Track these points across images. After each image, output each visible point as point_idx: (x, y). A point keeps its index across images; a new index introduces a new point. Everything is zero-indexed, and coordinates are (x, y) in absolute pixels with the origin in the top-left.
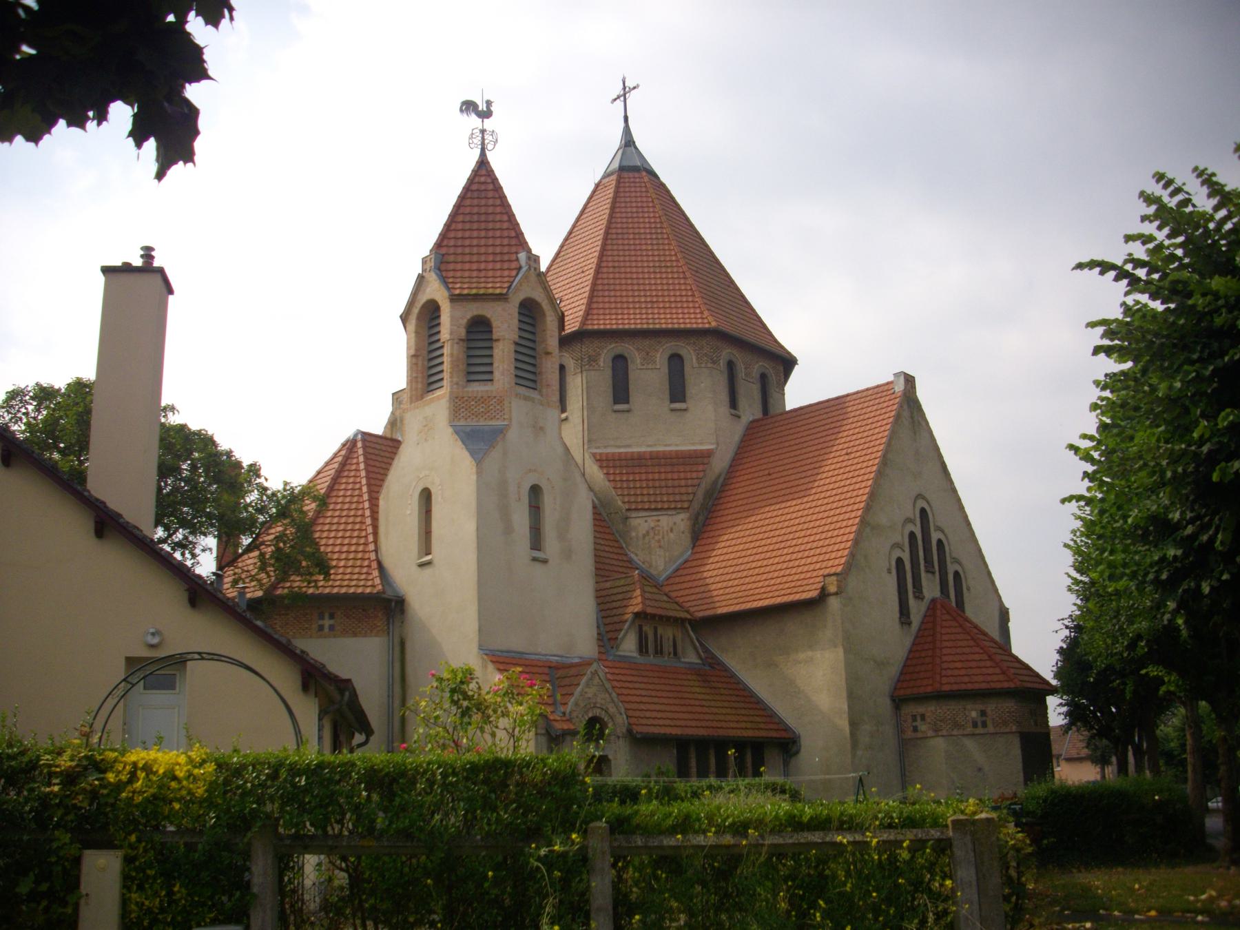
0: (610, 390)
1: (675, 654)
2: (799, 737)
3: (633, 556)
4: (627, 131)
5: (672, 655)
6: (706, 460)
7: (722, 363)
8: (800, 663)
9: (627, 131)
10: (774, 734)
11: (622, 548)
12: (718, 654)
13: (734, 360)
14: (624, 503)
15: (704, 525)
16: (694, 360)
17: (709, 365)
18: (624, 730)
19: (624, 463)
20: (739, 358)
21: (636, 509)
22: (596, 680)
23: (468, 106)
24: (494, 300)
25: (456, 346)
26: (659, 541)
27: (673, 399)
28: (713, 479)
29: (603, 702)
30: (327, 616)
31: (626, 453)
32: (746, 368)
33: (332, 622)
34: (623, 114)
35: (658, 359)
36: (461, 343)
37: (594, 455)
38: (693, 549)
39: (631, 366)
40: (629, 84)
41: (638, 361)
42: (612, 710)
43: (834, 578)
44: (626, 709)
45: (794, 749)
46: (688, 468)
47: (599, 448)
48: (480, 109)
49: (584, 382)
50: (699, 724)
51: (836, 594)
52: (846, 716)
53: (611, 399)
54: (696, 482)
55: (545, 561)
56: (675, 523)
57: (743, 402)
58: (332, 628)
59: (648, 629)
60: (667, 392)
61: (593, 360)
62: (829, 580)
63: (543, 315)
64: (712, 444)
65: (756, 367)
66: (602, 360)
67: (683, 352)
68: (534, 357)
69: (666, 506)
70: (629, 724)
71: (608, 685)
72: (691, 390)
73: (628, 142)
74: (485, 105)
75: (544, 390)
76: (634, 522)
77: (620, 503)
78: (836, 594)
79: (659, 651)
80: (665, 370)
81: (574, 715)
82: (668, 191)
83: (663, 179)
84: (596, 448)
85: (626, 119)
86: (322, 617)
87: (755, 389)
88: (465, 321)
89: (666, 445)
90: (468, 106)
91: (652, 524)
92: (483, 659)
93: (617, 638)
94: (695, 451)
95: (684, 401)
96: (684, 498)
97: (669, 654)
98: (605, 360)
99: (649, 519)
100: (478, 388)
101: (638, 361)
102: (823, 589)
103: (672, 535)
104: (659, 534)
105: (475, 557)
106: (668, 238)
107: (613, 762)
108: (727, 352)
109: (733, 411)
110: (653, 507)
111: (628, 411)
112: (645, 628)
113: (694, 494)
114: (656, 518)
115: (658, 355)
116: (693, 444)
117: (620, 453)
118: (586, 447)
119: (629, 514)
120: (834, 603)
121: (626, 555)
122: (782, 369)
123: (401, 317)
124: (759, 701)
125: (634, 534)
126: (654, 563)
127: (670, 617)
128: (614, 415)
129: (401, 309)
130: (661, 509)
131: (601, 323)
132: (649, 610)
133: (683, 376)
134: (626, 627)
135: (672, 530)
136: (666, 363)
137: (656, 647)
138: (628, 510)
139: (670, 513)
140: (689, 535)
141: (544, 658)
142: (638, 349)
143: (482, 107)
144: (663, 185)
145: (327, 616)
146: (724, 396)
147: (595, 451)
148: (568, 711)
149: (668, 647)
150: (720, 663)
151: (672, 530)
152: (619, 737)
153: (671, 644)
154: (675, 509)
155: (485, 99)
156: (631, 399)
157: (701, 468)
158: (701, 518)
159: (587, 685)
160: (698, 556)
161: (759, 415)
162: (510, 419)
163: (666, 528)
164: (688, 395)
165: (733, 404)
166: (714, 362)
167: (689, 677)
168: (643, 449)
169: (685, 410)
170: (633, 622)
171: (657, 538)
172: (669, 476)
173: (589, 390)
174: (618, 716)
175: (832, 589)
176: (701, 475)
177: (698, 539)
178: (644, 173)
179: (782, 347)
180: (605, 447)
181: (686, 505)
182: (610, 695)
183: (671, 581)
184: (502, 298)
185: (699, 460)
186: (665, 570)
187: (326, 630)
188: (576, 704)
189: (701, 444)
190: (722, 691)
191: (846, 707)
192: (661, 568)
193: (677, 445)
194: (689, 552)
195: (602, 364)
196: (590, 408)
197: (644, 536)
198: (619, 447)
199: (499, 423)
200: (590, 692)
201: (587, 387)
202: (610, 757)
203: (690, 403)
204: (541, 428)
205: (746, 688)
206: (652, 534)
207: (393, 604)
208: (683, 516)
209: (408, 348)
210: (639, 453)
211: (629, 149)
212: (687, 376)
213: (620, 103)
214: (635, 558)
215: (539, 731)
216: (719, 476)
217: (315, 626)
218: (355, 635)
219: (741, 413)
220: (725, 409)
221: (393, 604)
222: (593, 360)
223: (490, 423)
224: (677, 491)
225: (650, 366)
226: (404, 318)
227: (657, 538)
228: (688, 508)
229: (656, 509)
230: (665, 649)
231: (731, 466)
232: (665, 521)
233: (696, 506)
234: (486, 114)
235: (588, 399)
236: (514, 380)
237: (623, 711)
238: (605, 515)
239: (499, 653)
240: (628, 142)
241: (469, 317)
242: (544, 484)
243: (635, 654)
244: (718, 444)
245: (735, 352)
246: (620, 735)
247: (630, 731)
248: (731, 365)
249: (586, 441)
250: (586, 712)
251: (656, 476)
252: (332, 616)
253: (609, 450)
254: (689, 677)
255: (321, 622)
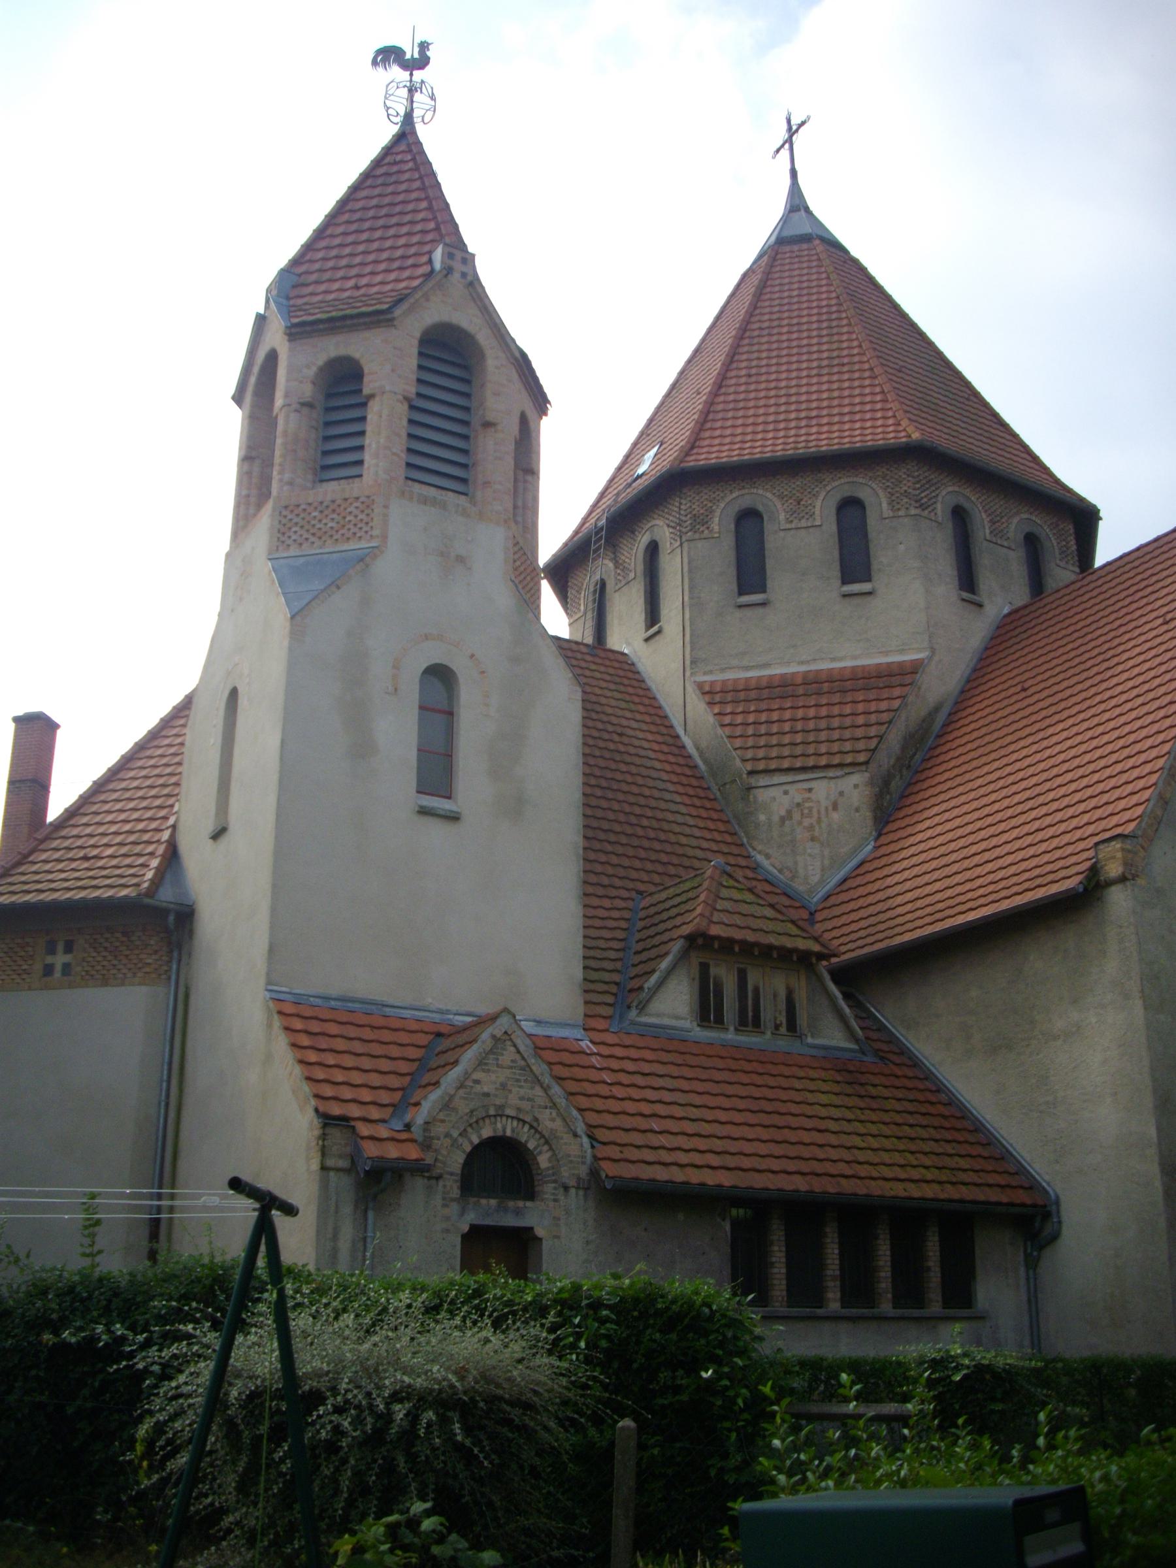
0: (732, 572)
1: (792, 1026)
2: (1057, 1202)
3: (760, 858)
4: (795, 191)
5: (783, 1030)
6: (908, 679)
7: (941, 510)
8: (1056, 1038)
9: (795, 191)
10: (994, 1196)
11: (742, 845)
12: (899, 1032)
13: (967, 505)
14: (744, 761)
15: (903, 797)
16: (885, 505)
17: (913, 511)
18: (583, 1171)
19: (753, 695)
20: (980, 507)
21: (766, 771)
22: (508, 1055)
23: (388, 55)
24: (368, 326)
25: (293, 416)
26: (811, 828)
27: (847, 577)
28: (923, 713)
29: (525, 1105)
30: (60, 947)
31: (759, 678)
32: (992, 522)
33: (67, 958)
34: (789, 167)
35: (817, 511)
36: (305, 410)
37: (700, 686)
38: (876, 839)
39: (768, 527)
40: (795, 121)
41: (782, 516)
42: (549, 1122)
43: (1117, 845)
44: (589, 1126)
45: (1048, 1230)
46: (872, 695)
47: (711, 672)
48: (408, 56)
49: (686, 560)
50: (791, 1166)
51: (1123, 879)
52: (1152, 1152)
53: (735, 587)
54: (885, 717)
55: (453, 818)
56: (841, 794)
57: (987, 581)
58: (67, 968)
59: (725, 974)
60: (836, 566)
61: (700, 522)
62: (1106, 851)
63: (481, 355)
64: (920, 650)
65: (1015, 520)
66: (716, 520)
67: (864, 494)
68: (466, 437)
69: (823, 761)
70: (596, 1158)
71: (539, 1068)
72: (881, 557)
73: (797, 204)
74: (416, 50)
75: (479, 494)
76: (762, 795)
77: (738, 762)
78: (1123, 879)
79: (750, 1020)
80: (832, 527)
81: (439, 1129)
82: (862, 270)
83: (854, 252)
84: (705, 674)
85: (794, 173)
86: (52, 951)
87: (1016, 562)
88: (314, 369)
89: (833, 660)
90: (388, 55)
91: (798, 799)
92: (268, 1007)
93: (641, 988)
94: (889, 664)
95: (869, 580)
96: (861, 745)
97: (777, 1027)
98: (721, 519)
99: (791, 789)
100: (332, 491)
101: (782, 516)
102: (1094, 871)
103: (835, 816)
104: (810, 816)
105: (272, 799)
106: (849, 325)
107: (546, 1245)
108: (949, 493)
109: (965, 595)
110: (798, 765)
111: (763, 604)
112: (713, 971)
113: (881, 737)
114: (806, 785)
115: (818, 504)
116: (886, 653)
117: (747, 679)
118: (688, 674)
119: (753, 781)
120: (1119, 900)
121: (749, 857)
122: (1070, 528)
123: (233, 398)
124: (978, 1127)
125: (762, 818)
126: (801, 872)
127: (771, 947)
128: (739, 614)
129: (232, 387)
130: (815, 768)
131: (709, 456)
132: (715, 930)
133: (866, 535)
134: (664, 964)
135: (835, 807)
136: (833, 519)
137: (743, 1011)
138: (751, 773)
139: (831, 773)
140: (869, 814)
141: (437, 1017)
142: (781, 497)
143: (411, 52)
144: (856, 263)
145: (60, 947)
146: (946, 565)
147: (701, 678)
148: (420, 1121)
149: (774, 1011)
150: (903, 1051)
151: (835, 807)
152: (566, 1188)
153: (782, 1006)
154: (840, 765)
155: (417, 41)
156: (769, 584)
157: (897, 692)
158: (896, 784)
159: (481, 1064)
160: (883, 851)
161: (1019, 595)
162: (384, 537)
163: (824, 803)
164: (875, 566)
165: (968, 580)
166: (923, 507)
167: (812, 1074)
168: (793, 669)
169: (870, 593)
170: (684, 955)
171: (806, 822)
172: (836, 710)
173: (692, 571)
174: (567, 1138)
175: (1113, 870)
176: (896, 703)
177: (887, 823)
178: (817, 242)
179: (1057, 481)
180: (723, 670)
181: (862, 758)
182: (546, 1090)
183: (832, 901)
184: (379, 319)
185: (896, 680)
186: (822, 882)
187: (58, 974)
188: (447, 1105)
189: (902, 651)
190: (890, 1104)
191: (1153, 1132)
192: (815, 879)
193: (854, 658)
194: (870, 847)
195: (716, 528)
196: (695, 604)
197: (783, 820)
198: (747, 668)
199: (363, 544)
200: (489, 1082)
201: (690, 571)
202: (540, 1232)
203: (879, 582)
204: (460, 559)
205: (952, 1102)
206: (796, 816)
207: (171, 918)
208: (858, 778)
209: (240, 449)
210: (782, 675)
211: (795, 216)
212: (872, 534)
213: (785, 153)
214: (766, 863)
215: (330, 1163)
216: (937, 709)
217: (38, 967)
218: (105, 982)
219: (984, 598)
220: (947, 590)
221: (171, 918)
222: (700, 522)
223: (346, 547)
224: (847, 734)
225: (803, 523)
226: (238, 398)
227: (806, 822)
228: (866, 763)
229: (804, 769)
230: (767, 1015)
231: (962, 692)
232: (822, 790)
233: (885, 760)
234: (422, 62)
235: (691, 588)
236: (401, 472)
237: (580, 1128)
238: (715, 788)
239: (319, 1002)
240: (797, 204)
241: (320, 363)
242: (459, 665)
243: (686, 1024)
244: (933, 651)
245: (967, 492)
246: (572, 1183)
247: (594, 1173)
248: (960, 515)
249: (688, 663)
250: (477, 1124)
251: (812, 712)
252: (69, 948)
253: (730, 675)
254: (812, 1074)
255: (49, 960)
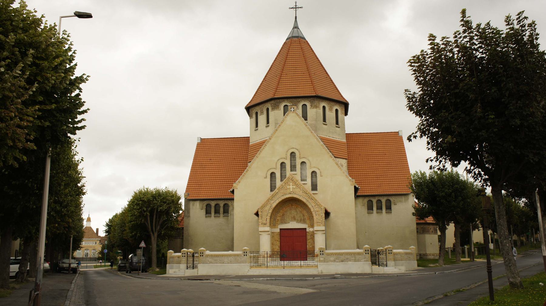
73: (296, 27)
85: (296, 17)
240: (296, 27)
